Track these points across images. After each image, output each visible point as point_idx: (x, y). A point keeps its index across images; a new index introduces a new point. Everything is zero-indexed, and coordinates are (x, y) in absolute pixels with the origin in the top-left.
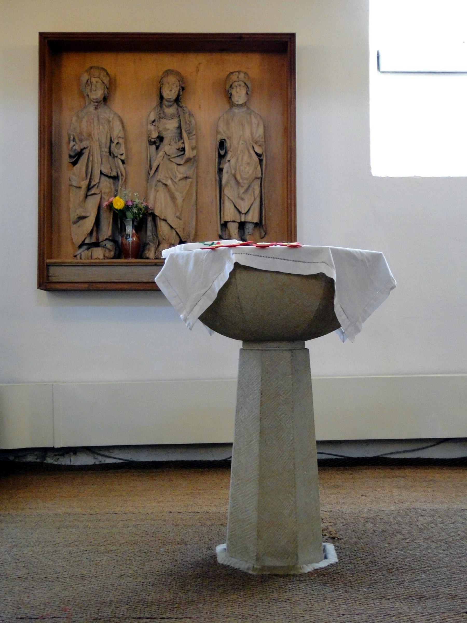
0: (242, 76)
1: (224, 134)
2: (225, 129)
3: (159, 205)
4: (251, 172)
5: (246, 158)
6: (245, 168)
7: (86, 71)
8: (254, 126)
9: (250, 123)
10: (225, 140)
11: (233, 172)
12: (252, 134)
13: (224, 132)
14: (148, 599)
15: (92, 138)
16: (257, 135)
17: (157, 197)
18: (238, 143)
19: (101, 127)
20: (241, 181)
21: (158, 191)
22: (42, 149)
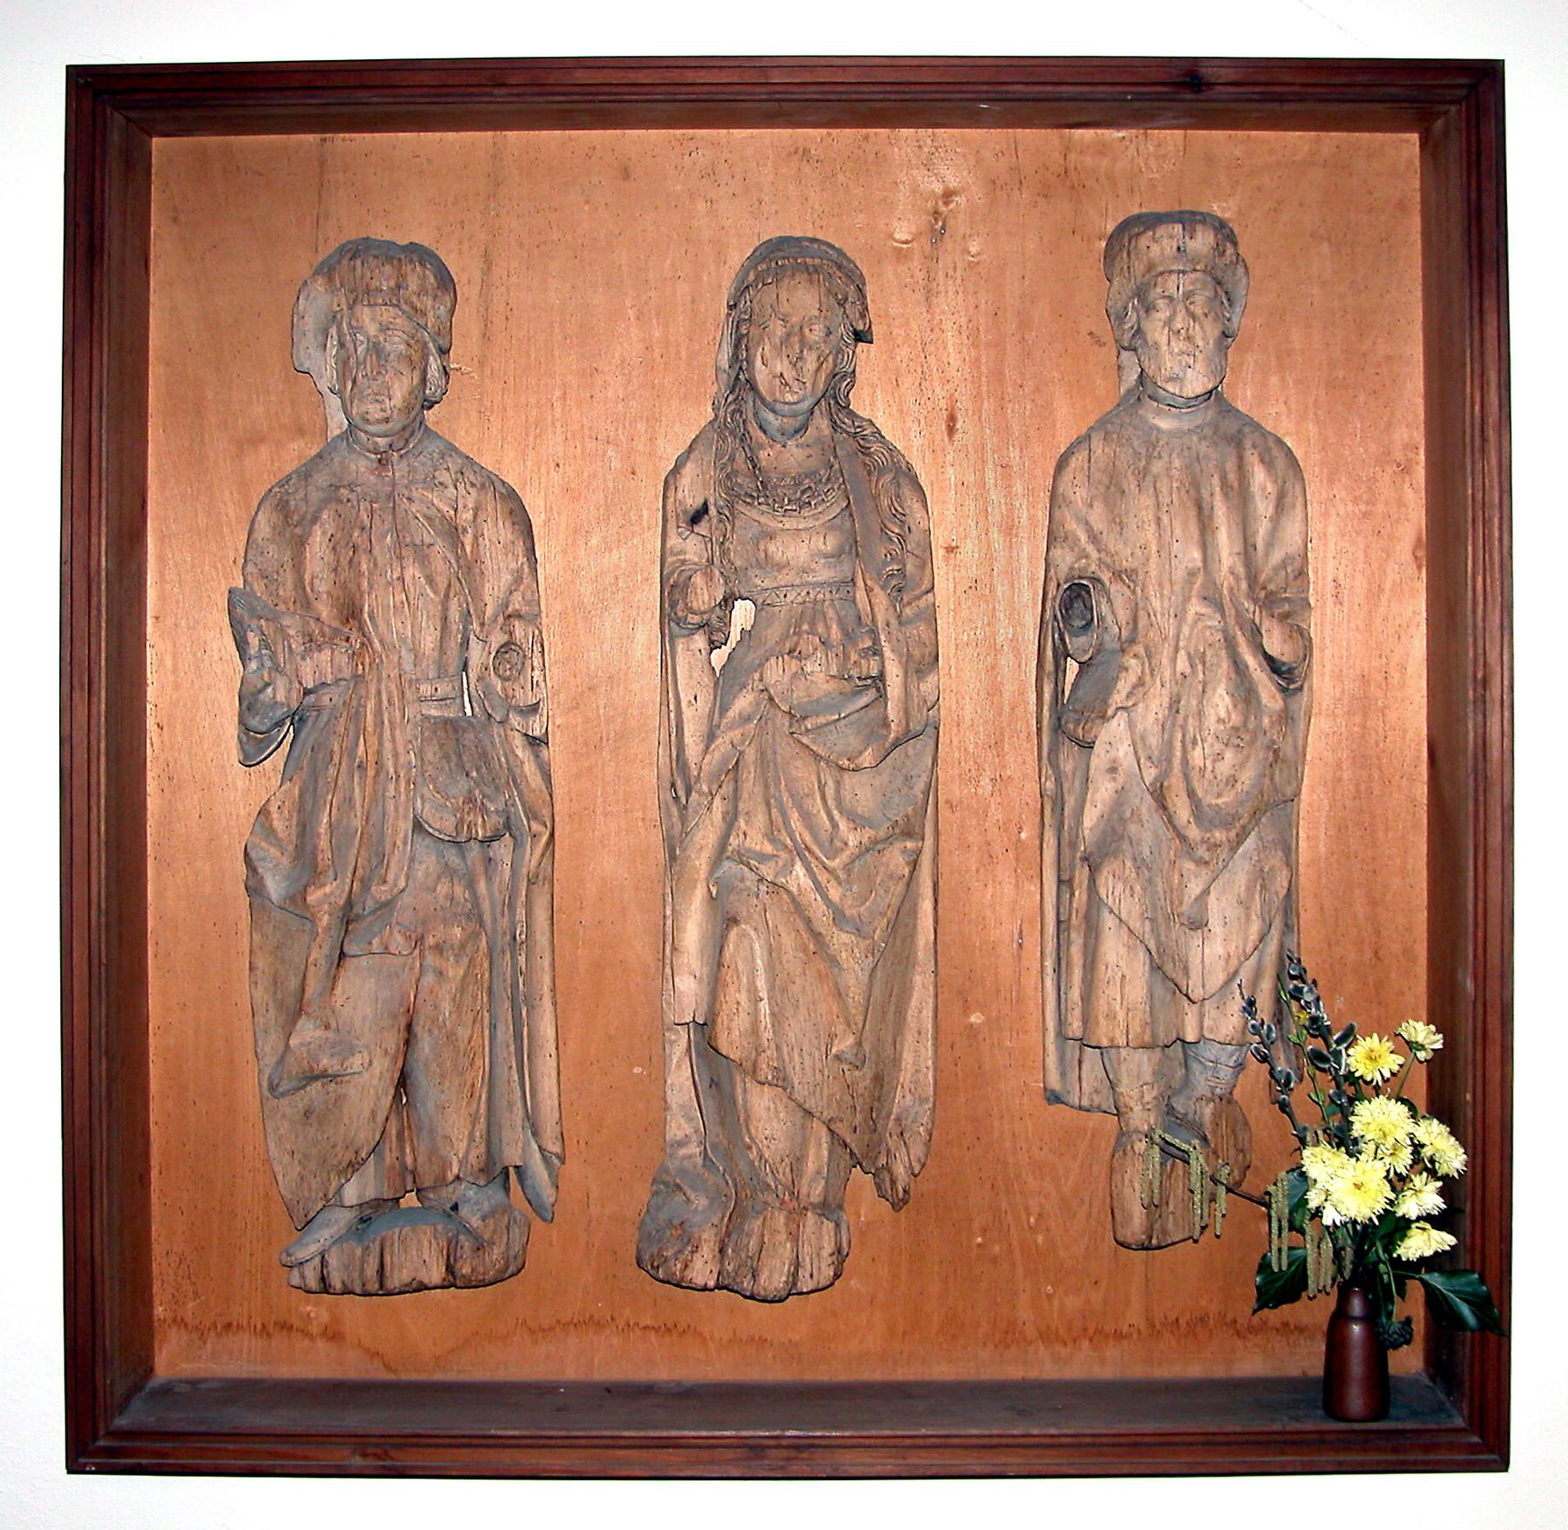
0: (1202, 241)
1: (1090, 549)
2: (1097, 517)
3: (743, 998)
4: (1247, 777)
5: (1221, 702)
6: (1219, 757)
7: (327, 270)
8: (1263, 508)
9: (1240, 497)
10: (1096, 580)
11: (1150, 774)
12: (1247, 550)
13: (1094, 538)
14: (682, 552)
15: (361, 629)
16: (1277, 557)
17: (727, 954)
18: (1179, 616)
19: (413, 572)
20: (1194, 833)
21: (733, 921)
22: (80, 697)
